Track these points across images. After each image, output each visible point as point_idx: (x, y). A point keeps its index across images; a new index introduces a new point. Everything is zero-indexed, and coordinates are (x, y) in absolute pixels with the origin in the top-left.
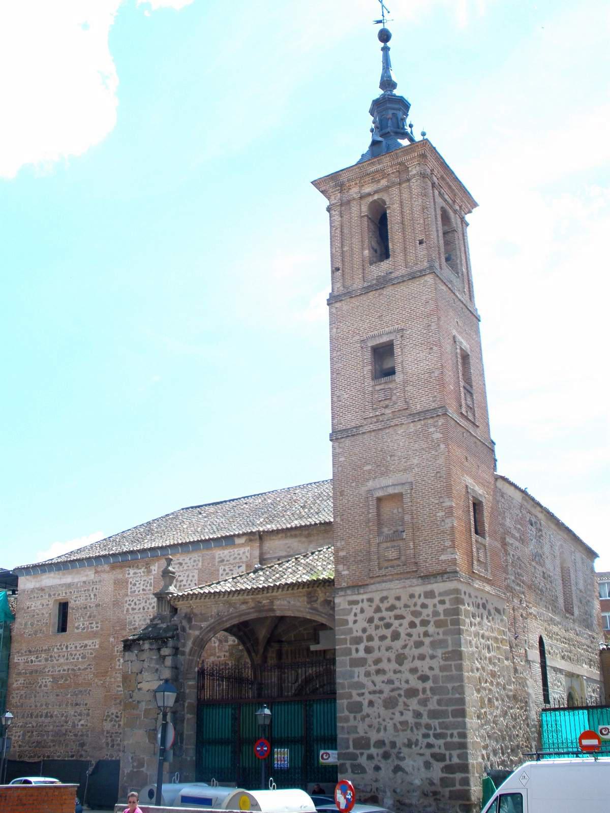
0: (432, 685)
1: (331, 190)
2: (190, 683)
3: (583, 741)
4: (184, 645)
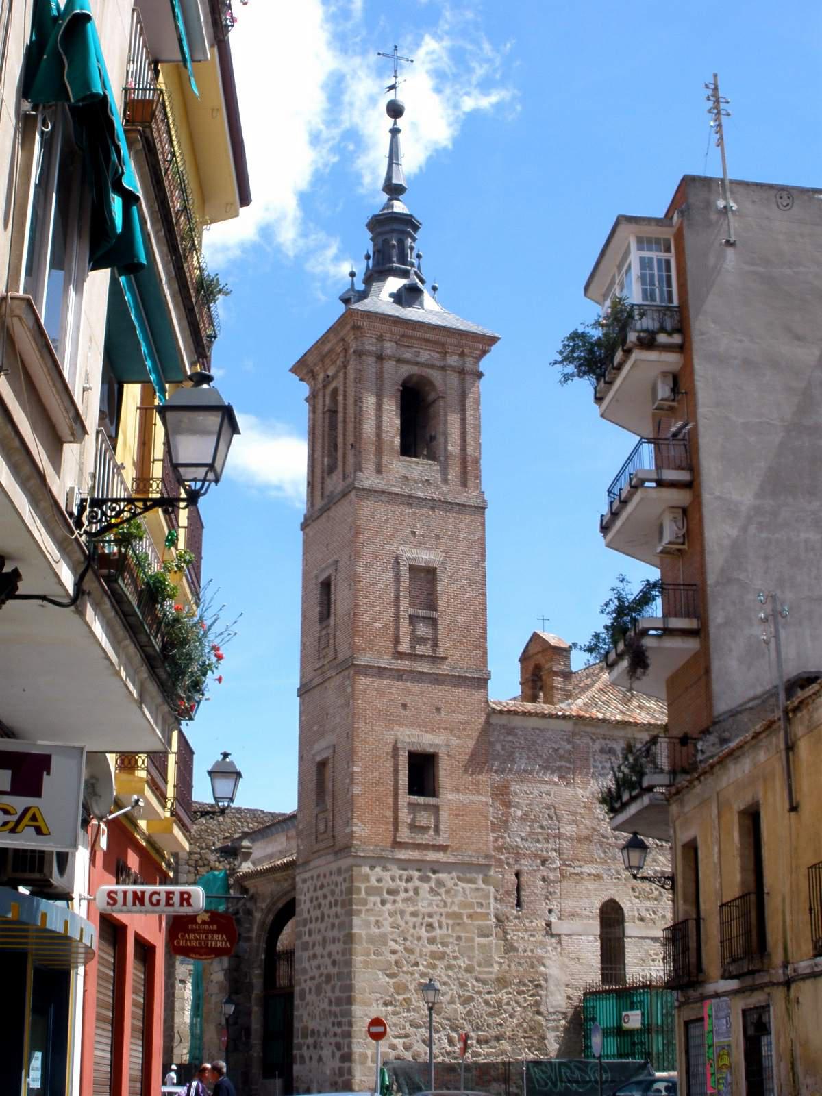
4: (250, 930)
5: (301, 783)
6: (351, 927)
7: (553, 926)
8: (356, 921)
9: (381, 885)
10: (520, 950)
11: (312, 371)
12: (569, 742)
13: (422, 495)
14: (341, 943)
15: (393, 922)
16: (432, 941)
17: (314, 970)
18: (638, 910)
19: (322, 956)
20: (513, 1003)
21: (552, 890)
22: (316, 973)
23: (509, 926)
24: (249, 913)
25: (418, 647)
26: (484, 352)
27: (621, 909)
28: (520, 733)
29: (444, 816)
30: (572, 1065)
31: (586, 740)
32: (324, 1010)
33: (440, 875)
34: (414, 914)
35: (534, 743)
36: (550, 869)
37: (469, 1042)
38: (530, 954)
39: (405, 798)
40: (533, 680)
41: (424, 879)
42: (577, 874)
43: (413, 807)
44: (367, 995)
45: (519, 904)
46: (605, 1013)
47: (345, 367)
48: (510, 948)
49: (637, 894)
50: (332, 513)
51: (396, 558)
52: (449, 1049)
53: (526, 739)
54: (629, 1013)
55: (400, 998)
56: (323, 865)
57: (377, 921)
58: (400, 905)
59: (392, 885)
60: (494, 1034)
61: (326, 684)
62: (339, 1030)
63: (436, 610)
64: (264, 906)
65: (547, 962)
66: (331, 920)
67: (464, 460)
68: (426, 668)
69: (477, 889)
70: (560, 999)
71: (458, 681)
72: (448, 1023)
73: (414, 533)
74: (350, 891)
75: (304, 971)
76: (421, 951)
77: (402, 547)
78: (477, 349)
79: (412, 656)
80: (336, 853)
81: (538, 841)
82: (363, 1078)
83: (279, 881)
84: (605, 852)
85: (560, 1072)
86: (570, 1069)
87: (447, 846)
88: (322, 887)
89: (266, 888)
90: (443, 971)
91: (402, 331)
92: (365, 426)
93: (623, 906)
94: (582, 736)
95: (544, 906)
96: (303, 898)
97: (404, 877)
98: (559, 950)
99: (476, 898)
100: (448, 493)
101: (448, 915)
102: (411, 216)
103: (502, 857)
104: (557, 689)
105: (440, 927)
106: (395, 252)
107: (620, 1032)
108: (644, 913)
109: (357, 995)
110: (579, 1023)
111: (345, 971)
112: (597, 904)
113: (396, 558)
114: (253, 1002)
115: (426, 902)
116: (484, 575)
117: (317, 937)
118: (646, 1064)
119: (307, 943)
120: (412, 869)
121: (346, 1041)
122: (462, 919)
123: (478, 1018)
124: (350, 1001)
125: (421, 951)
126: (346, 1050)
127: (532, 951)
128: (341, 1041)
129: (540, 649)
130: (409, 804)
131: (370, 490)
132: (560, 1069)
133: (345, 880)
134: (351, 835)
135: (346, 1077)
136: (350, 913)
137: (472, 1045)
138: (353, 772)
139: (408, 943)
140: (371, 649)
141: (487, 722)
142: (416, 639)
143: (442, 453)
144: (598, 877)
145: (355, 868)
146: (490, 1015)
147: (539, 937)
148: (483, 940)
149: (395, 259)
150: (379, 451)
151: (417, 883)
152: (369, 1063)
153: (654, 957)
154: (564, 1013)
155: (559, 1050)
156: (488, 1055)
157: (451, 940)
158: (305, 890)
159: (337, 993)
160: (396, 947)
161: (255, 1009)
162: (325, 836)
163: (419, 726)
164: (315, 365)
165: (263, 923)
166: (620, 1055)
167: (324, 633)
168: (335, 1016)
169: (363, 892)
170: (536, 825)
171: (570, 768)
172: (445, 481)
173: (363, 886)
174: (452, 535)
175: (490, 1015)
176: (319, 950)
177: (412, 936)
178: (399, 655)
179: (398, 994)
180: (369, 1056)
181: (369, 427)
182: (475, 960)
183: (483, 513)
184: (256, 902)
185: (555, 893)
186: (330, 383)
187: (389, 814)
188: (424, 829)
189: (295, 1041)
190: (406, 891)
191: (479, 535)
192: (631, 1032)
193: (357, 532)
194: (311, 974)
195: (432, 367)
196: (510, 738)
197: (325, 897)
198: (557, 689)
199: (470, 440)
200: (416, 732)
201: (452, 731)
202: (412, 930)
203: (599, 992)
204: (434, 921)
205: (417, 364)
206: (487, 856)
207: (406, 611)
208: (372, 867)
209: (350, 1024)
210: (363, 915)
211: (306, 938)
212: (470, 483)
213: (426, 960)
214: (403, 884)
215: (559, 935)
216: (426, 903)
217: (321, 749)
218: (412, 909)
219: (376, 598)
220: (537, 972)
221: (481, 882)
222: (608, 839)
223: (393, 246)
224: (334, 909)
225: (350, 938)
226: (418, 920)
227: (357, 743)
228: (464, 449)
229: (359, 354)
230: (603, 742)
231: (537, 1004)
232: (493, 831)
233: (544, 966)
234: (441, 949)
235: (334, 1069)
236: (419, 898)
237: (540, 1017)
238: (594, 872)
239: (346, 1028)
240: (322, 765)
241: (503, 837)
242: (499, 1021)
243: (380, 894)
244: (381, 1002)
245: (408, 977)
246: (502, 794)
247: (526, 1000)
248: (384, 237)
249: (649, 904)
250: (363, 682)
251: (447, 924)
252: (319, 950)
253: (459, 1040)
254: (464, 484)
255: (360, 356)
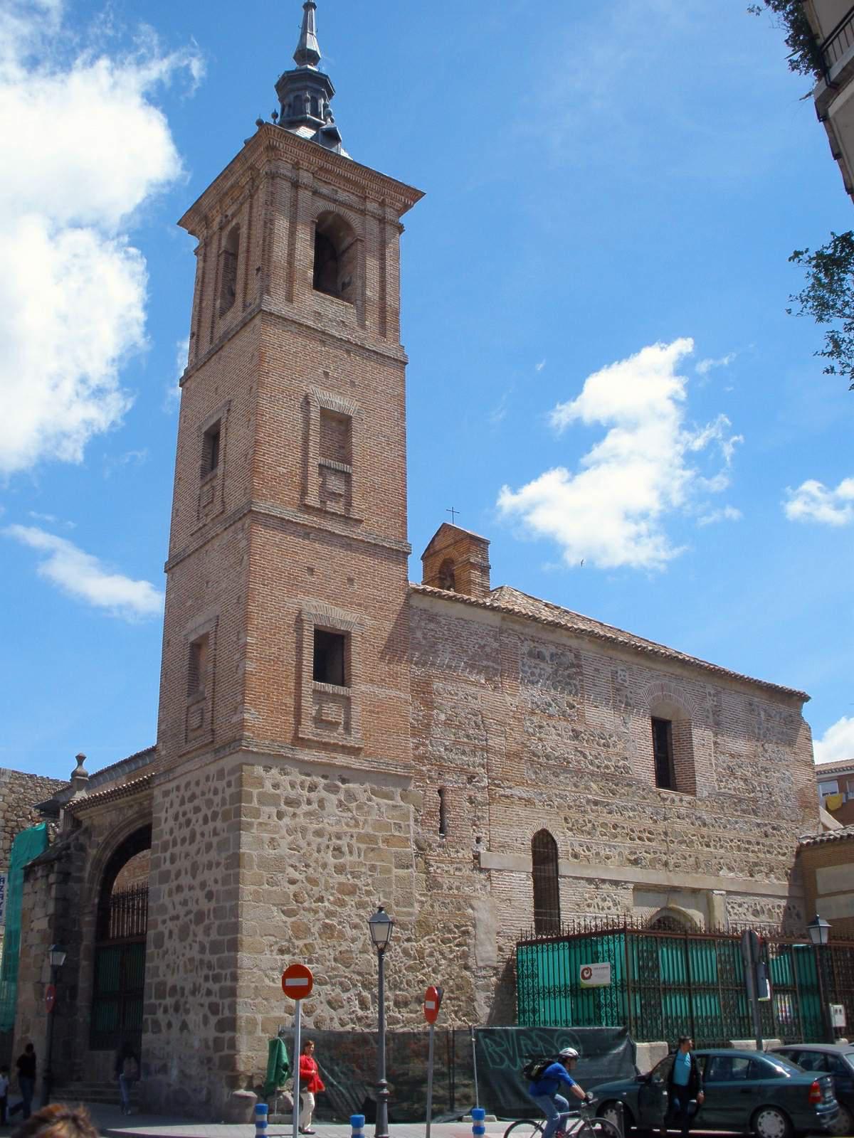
0: (215, 905)
1: (198, 228)
2: (87, 919)
3: (287, 980)
4: (82, 869)
5: (164, 674)
6: (238, 846)
7: (482, 859)
8: (246, 837)
9: (278, 792)
10: (445, 887)
11: (206, 218)
12: (496, 640)
13: (337, 334)
14: (222, 868)
15: (292, 842)
16: (340, 869)
17: (178, 907)
18: (572, 844)
19: (191, 888)
20: (437, 954)
21: (480, 814)
22: (181, 911)
23: (432, 855)
24: (82, 848)
25: (328, 503)
26: (406, 207)
27: (554, 841)
28: (444, 622)
29: (357, 710)
30: (533, 1035)
31: (515, 640)
32: (191, 960)
33: (351, 785)
34: (319, 833)
35: (459, 636)
36: (478, 788)
37: (386, 1004)
38: (456, 892)
39: (309, 684)
40: (440, 578)
41: (333, 789)
42: (507, 797)
43: (319, 696)
44: (258, 938)
45: (442, 830)
46: (552, 967)
47: (251, 196)
48: (433, 884)
49: (570, 825)
50: (223, 353)
51: (306, 397)
52: (360, 1013)
53: (449, 630)
54: (591, 966)
55: (300, 943)
56: (197, 769)
57: (273, 839)
58: (301, 820)
59: (292, 794)
60: (415, 994)
61: (208, 547)
62: (215, 987)
63: (351, 465)
64: (100, 840)
65: (475, 903)
66: (207, 839)
67: (383, 310)
68: (338, 529)
69: (395, 807)
70: (489, 951)
71: (373, 549)
72: (359, 978)
73: (326, 374)
74: (238, 797)
75: (163, 909)
76: (326, 881)
77: (311, 386)
78: (399, 201)
79: (321, 512)
80: (216, 751)
81: (464, 753)
82: (249, 1054)
83: (121, 809)
84: (536, 773)
85: (519, 1044)
86: (531, 1038)
87: (360, 749)
88: (193, 797)
89: (104, 819)
90: (354, 909)
91: (321, 163)
92: (276, 249)
93: (556, 838)
94: (509, 634)
95: (471, 833)
96: (163, 815)
97: (307, 784)
98: (488, 888)
99: (393, 818)
100: (365, 339)
101: (361, 838)
102: (327, 76)
103: (424, 768)
104: (475, 584)
105: (351, 852)
106: (308, 106)
107: (576, 991)
108: (578, 849)
109: (245, 939)
110: (513, 980)
111: (228, 905)
112: (530, 835)
113: (306, 397)
114: (82, 956)
115: (333, 819)
116: (404, 436)
117: (183, 864)
118: (625, 1031)
119: (169, 872)
120: (317, 775)
121: (227, 1001)
122: (377, 844)
123: (396, 972)
124: (234, 946)
125: (326, 881)
126: (227, 1013)
127: (458, 888)
128: (220, 1002)
129: (452, 541)
130: (315, 691)
131: (278, 317)
132: (518, 1039)
133: (229, 784)
134: (242, 724)
135: (226, 1052)
136: (238, 827)
137: (388, 1008)
138: (246, 644)
139: (311, 870)
140: (273, 497)
141: (407, 604)
142: (326, 494)
143: (359, 297)
144: (529, 802)
145: (245, 767)
146: (409, 968)
147: (466, 872)
148: (401, 872)
149: (309, 111)
150: (290, 279)
151: (324, 794)
152: (259, 1033)
153: (590, 901)
154: (495, 968)
155: (490, 1015)
156: (408, 1022)
157: (363, 870)
158: (168, 805)
159: (214, 936)
160: (296, 875)
161: (84, 963)
162: (200, 732)
163: (328, 597)
164: (211, 208)
165: (97, 862)
166: (576, 1022)
167: (207, 487)
168: (210, 967)
169: (255, 799)
170: (462, 733)
171: (497, 670)
172: (363, 327)
173: (255, 792)
174: (369, 385)
175: (409, 968)
176: (185, 880)
177: (316, 862)
178: (307, 509)
179: (297, 938)
180: (259, 1022)
181: (280, 251)
182: (392, 897)
183: (403, 369)
184: (90, 837)
185: (483, 818)
186: (228, 222)
187: (290, 701)
188: (332, 725)
189: (146, 1002)
190: (309, 802)
191: (399, 391)
192: (594, 991)
193: (261, 360)
194: (172, 912)
195: (350, 207)
196: (432, 626)
197: (197, 810)
198: (475, 584)
199: (389, 289)
200: (324, 603)
201: (366, 608)
202: (316, 855)
203: (531, 943)
204: (343, 843)
205: (335, 201)
206: (406, 767)
207: (315, 460)
208: (267, 768)
209: (235, 978)
210: (254, 831)
211: (167, 866)
212: (390, 334)
213: (332, 894)
214: (305, 793)
215: (488, 870)
216: (333, 820)
217: (197, 625)
218: (315, 826)
219: (279, 446)
220: (464, 915)
221: (399, 798)
222: (539, 757)
223: (307, 100)
224: (211, 825)
225: (236, 861)
226: (324, 841)
227: (252, 608)
228: (383, 298)
229: (273, 176)
230: (532, 645)
231: (465, 956)
232: (414, 736)
233: (473, 909)
234: (351, 881)
235: (206, 1041)
236: (324, 813)
237: (468, 973)
238: (524, 795)
239: (229, 983)
240: (197, 647)
241: (424, 745)
242: (421, 977)
243: (277, 804)
244: (275, 948)
245: (311, 916)
246: (422, 691)
247: (452, 952)
248: (296, 93)
249: (584, 838)
250: (262, 536)
251: (358, 848)
252: (185, 880)
253: (374, 1002)
254: (383, 333)
255: (273, 178)
